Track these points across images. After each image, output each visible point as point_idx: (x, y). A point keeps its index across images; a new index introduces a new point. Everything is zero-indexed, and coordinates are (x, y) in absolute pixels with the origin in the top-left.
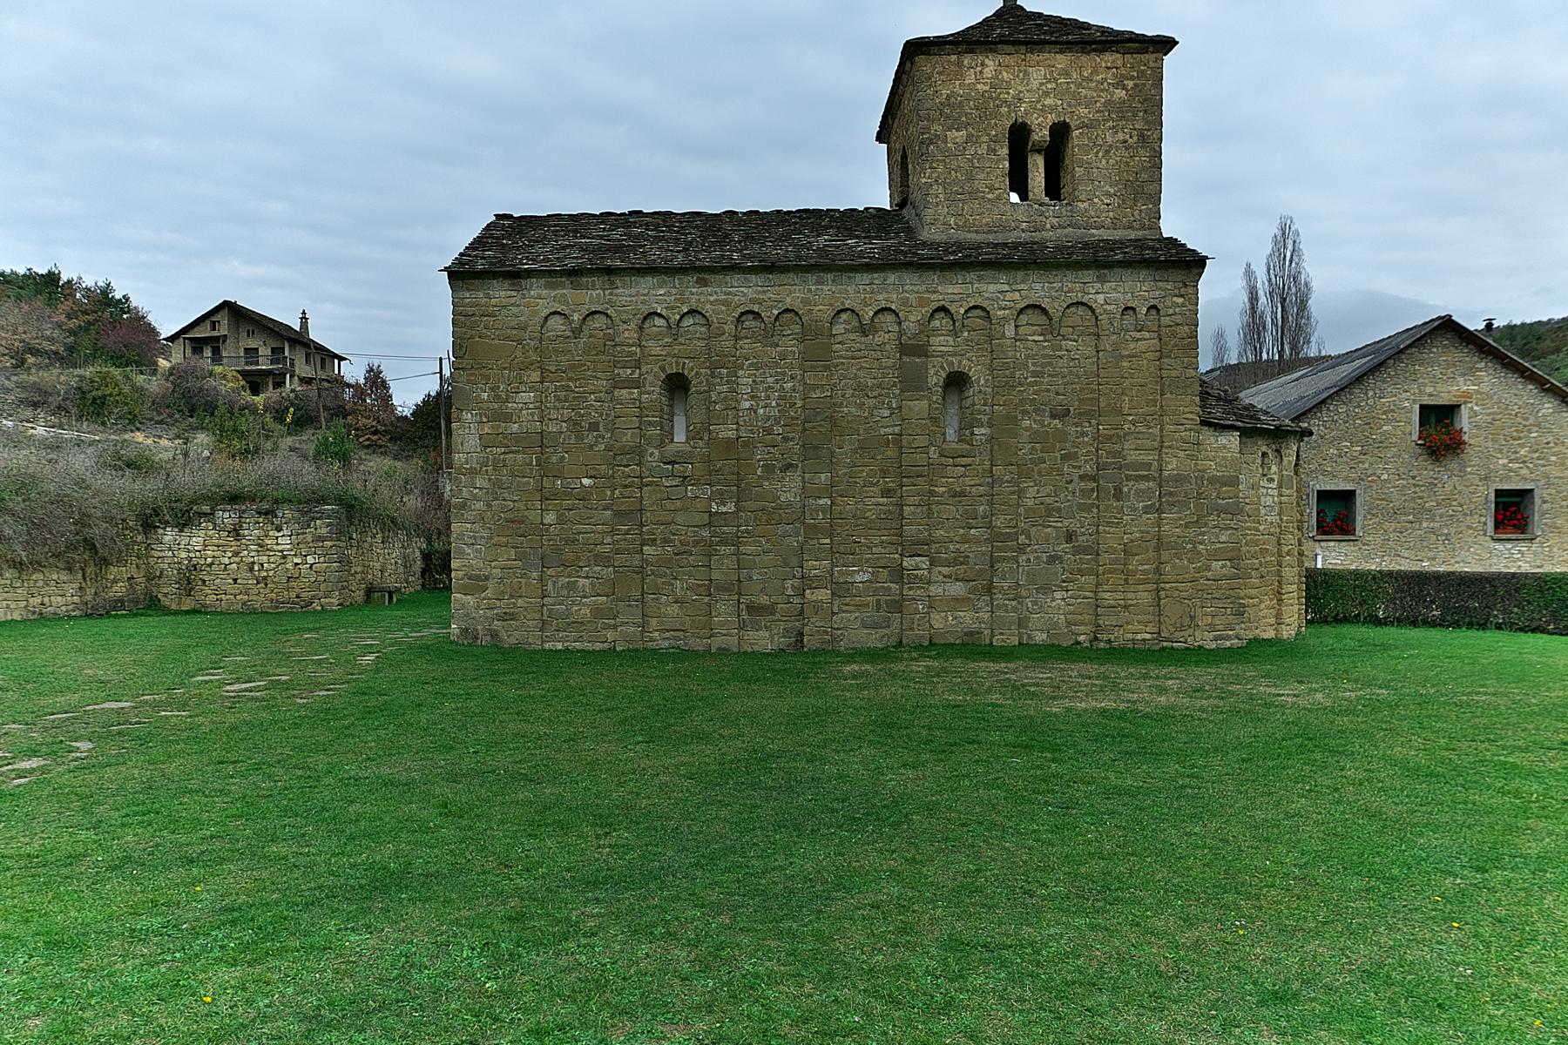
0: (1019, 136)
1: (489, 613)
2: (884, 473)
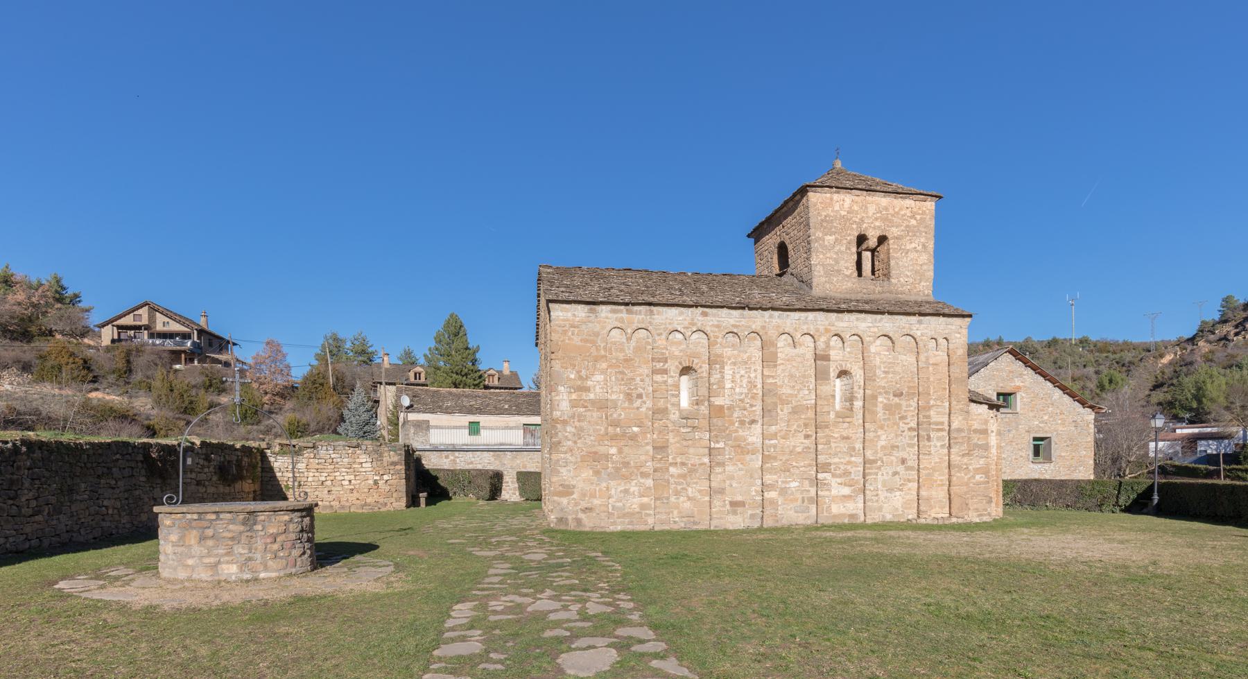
0: (861, 239)
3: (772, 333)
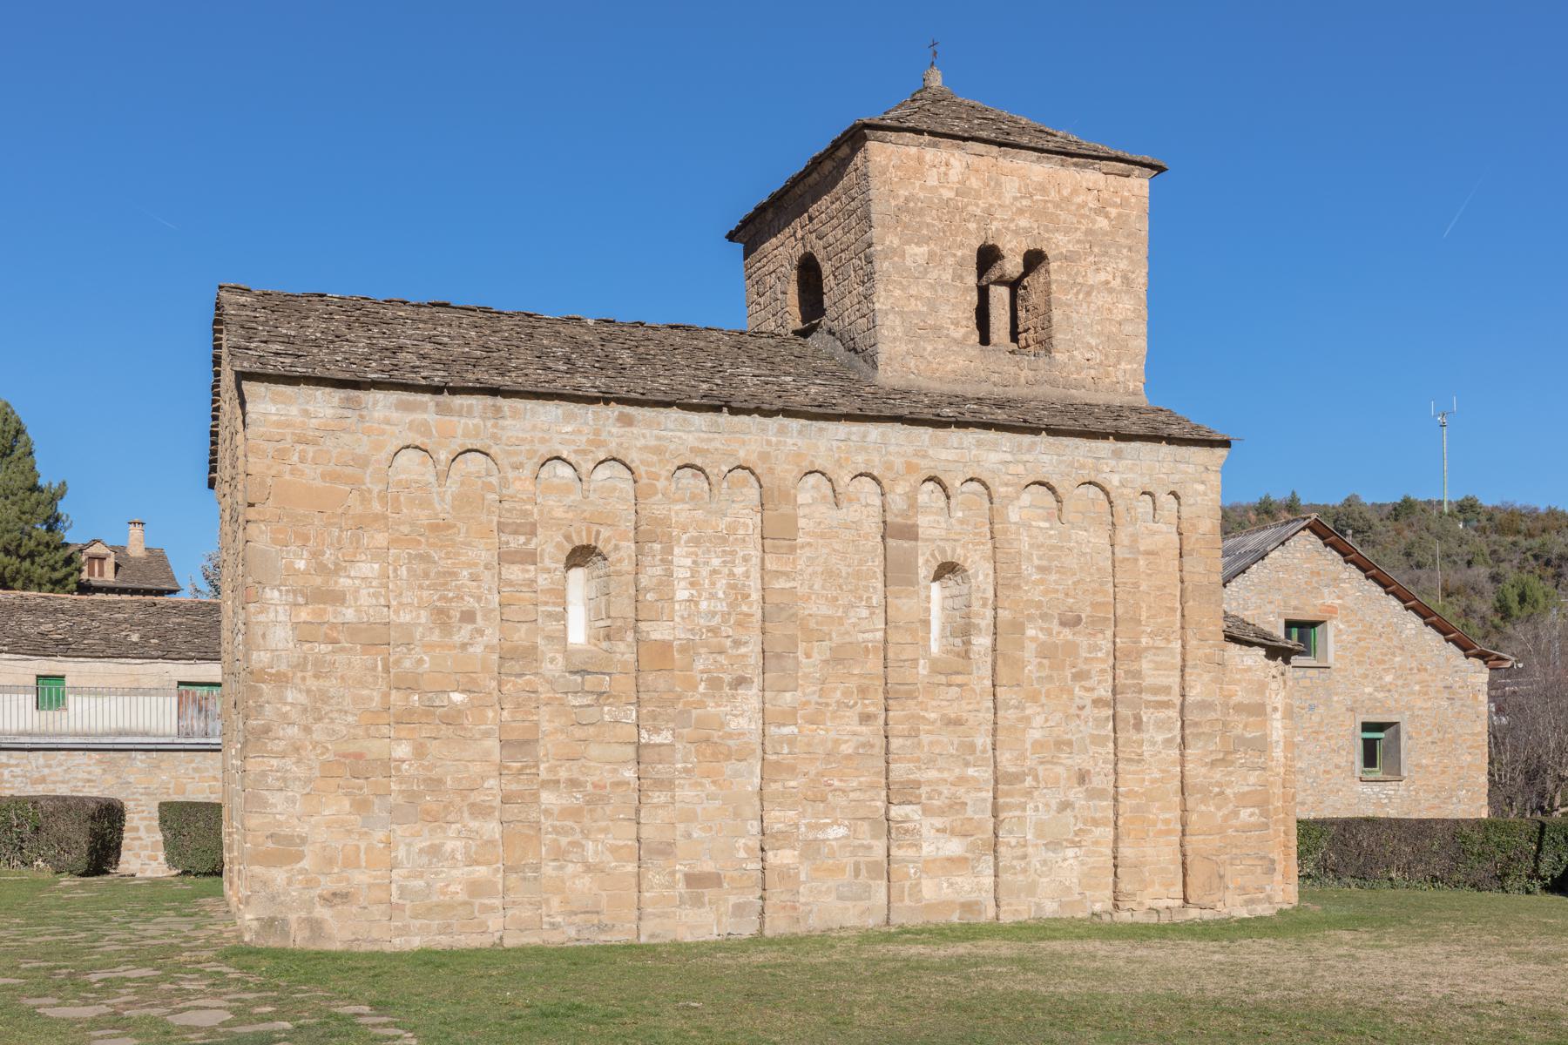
0: (988, 257)
2: (863, 691)
3: (785, 471)
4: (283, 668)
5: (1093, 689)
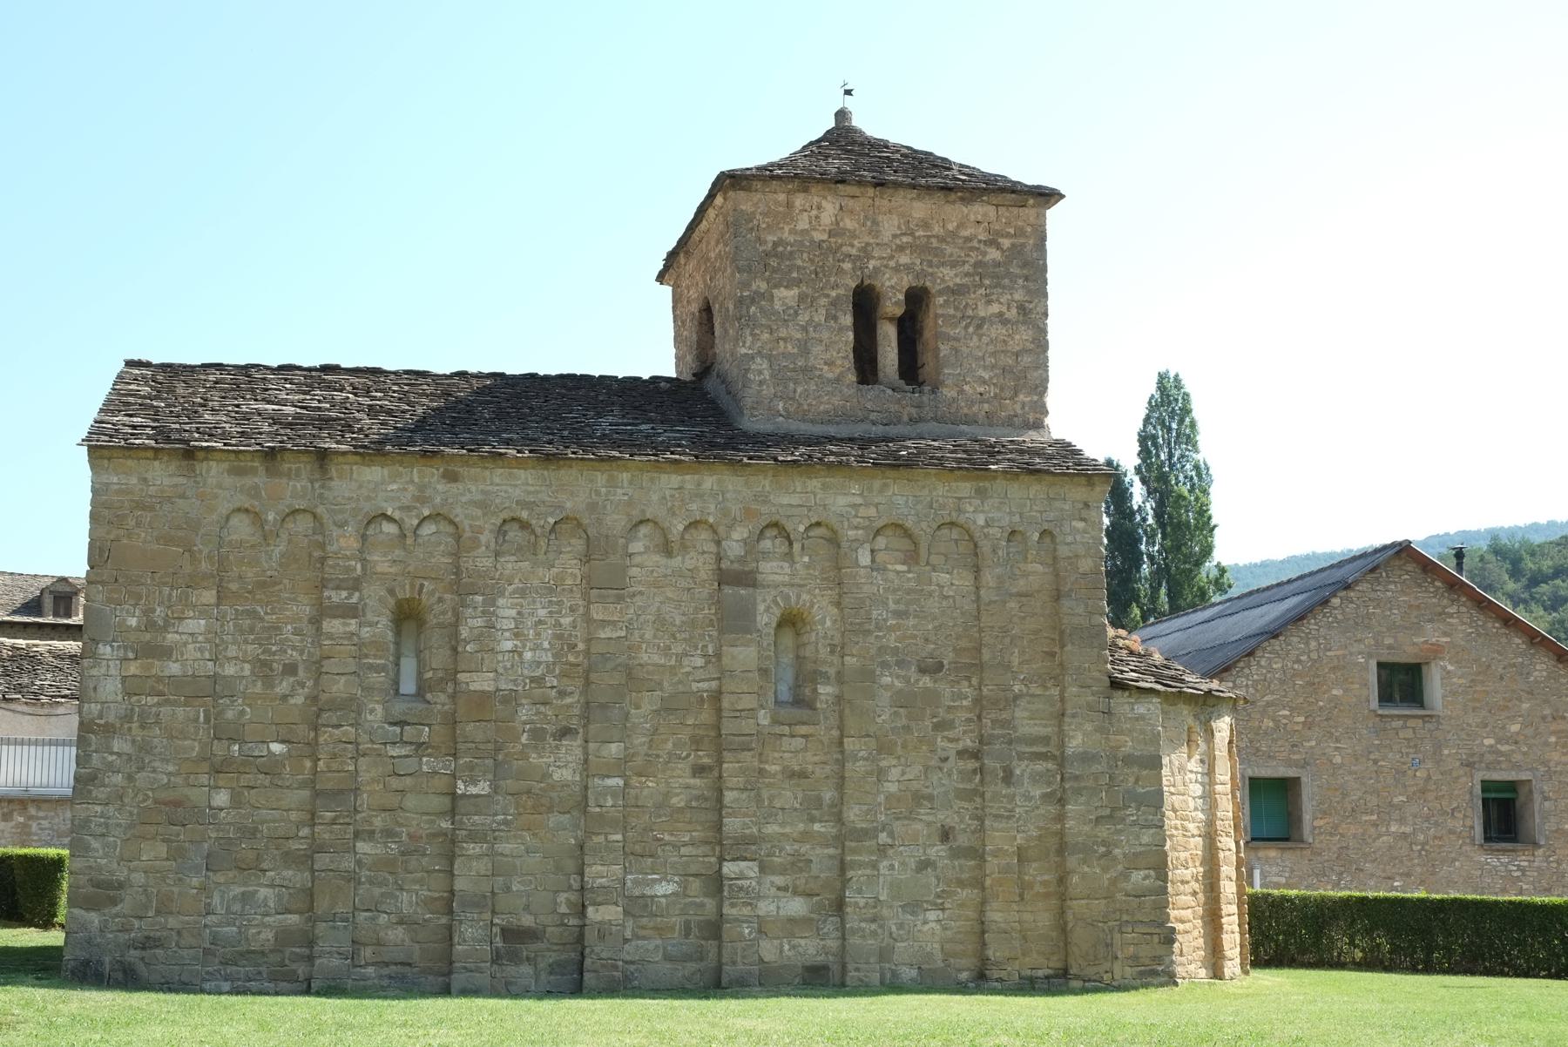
0: (865, 303)
1: (123, 937)
3: (616, 521)
4: (111, 719)
5: (958, 740)
